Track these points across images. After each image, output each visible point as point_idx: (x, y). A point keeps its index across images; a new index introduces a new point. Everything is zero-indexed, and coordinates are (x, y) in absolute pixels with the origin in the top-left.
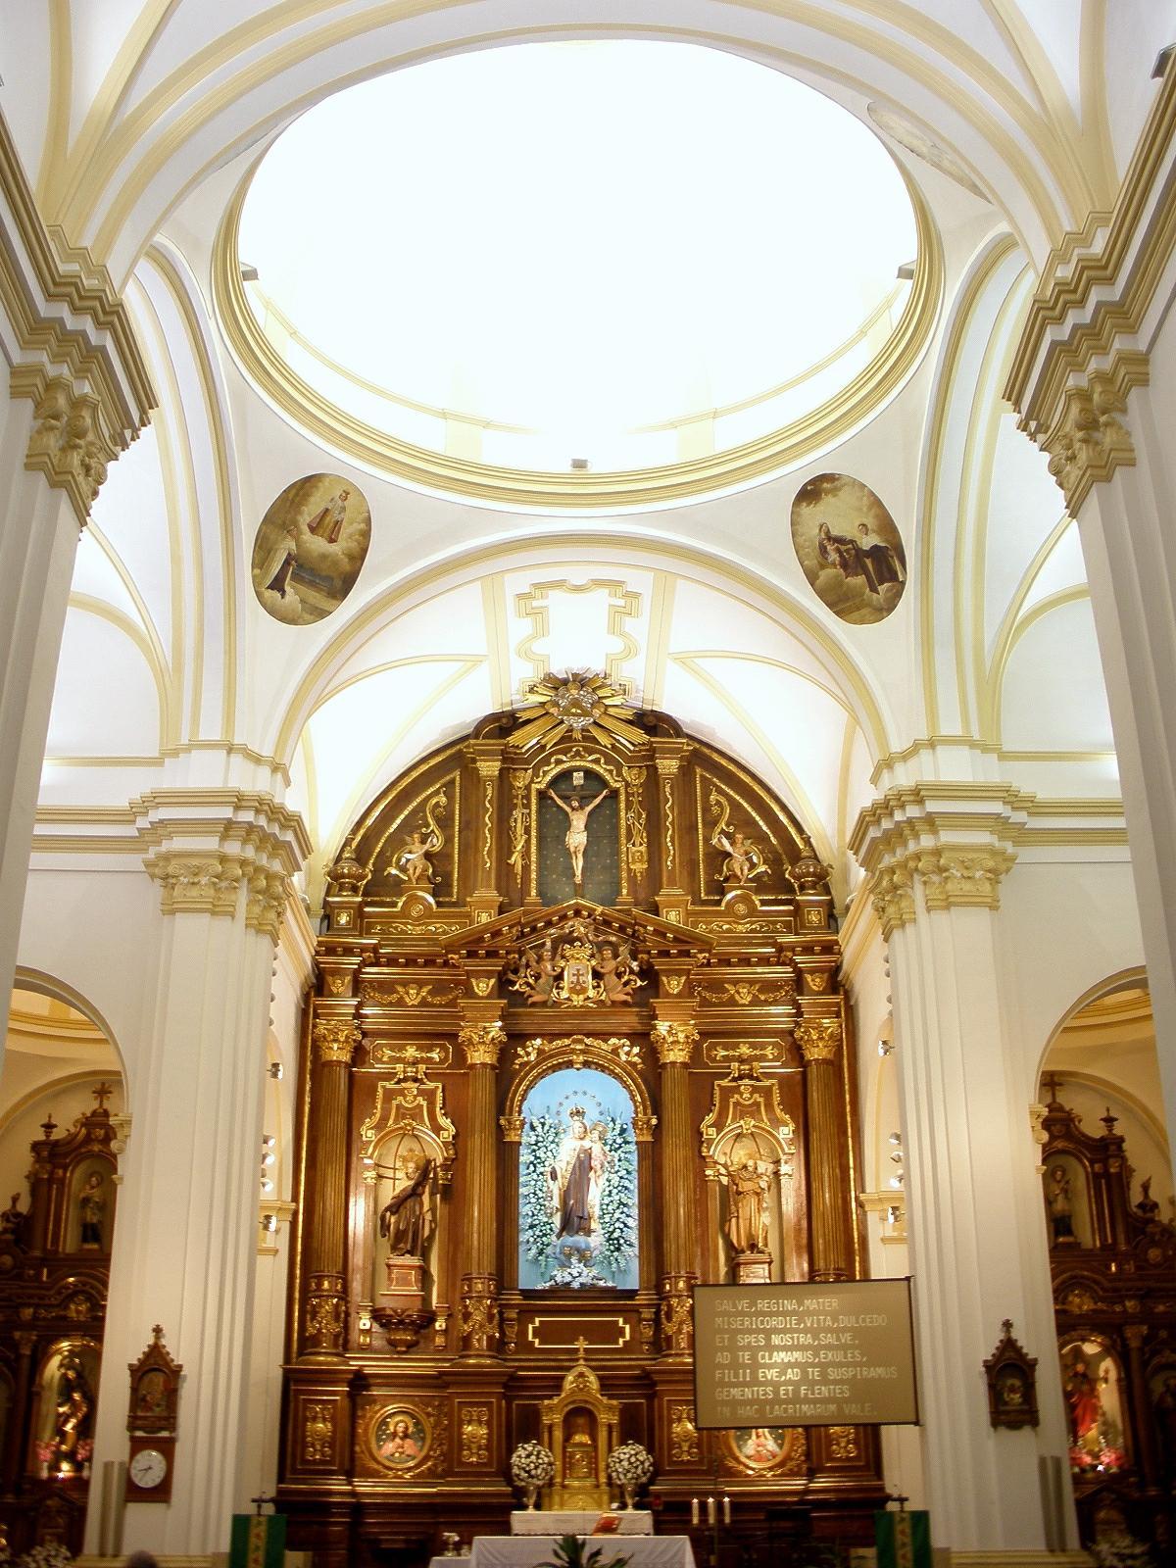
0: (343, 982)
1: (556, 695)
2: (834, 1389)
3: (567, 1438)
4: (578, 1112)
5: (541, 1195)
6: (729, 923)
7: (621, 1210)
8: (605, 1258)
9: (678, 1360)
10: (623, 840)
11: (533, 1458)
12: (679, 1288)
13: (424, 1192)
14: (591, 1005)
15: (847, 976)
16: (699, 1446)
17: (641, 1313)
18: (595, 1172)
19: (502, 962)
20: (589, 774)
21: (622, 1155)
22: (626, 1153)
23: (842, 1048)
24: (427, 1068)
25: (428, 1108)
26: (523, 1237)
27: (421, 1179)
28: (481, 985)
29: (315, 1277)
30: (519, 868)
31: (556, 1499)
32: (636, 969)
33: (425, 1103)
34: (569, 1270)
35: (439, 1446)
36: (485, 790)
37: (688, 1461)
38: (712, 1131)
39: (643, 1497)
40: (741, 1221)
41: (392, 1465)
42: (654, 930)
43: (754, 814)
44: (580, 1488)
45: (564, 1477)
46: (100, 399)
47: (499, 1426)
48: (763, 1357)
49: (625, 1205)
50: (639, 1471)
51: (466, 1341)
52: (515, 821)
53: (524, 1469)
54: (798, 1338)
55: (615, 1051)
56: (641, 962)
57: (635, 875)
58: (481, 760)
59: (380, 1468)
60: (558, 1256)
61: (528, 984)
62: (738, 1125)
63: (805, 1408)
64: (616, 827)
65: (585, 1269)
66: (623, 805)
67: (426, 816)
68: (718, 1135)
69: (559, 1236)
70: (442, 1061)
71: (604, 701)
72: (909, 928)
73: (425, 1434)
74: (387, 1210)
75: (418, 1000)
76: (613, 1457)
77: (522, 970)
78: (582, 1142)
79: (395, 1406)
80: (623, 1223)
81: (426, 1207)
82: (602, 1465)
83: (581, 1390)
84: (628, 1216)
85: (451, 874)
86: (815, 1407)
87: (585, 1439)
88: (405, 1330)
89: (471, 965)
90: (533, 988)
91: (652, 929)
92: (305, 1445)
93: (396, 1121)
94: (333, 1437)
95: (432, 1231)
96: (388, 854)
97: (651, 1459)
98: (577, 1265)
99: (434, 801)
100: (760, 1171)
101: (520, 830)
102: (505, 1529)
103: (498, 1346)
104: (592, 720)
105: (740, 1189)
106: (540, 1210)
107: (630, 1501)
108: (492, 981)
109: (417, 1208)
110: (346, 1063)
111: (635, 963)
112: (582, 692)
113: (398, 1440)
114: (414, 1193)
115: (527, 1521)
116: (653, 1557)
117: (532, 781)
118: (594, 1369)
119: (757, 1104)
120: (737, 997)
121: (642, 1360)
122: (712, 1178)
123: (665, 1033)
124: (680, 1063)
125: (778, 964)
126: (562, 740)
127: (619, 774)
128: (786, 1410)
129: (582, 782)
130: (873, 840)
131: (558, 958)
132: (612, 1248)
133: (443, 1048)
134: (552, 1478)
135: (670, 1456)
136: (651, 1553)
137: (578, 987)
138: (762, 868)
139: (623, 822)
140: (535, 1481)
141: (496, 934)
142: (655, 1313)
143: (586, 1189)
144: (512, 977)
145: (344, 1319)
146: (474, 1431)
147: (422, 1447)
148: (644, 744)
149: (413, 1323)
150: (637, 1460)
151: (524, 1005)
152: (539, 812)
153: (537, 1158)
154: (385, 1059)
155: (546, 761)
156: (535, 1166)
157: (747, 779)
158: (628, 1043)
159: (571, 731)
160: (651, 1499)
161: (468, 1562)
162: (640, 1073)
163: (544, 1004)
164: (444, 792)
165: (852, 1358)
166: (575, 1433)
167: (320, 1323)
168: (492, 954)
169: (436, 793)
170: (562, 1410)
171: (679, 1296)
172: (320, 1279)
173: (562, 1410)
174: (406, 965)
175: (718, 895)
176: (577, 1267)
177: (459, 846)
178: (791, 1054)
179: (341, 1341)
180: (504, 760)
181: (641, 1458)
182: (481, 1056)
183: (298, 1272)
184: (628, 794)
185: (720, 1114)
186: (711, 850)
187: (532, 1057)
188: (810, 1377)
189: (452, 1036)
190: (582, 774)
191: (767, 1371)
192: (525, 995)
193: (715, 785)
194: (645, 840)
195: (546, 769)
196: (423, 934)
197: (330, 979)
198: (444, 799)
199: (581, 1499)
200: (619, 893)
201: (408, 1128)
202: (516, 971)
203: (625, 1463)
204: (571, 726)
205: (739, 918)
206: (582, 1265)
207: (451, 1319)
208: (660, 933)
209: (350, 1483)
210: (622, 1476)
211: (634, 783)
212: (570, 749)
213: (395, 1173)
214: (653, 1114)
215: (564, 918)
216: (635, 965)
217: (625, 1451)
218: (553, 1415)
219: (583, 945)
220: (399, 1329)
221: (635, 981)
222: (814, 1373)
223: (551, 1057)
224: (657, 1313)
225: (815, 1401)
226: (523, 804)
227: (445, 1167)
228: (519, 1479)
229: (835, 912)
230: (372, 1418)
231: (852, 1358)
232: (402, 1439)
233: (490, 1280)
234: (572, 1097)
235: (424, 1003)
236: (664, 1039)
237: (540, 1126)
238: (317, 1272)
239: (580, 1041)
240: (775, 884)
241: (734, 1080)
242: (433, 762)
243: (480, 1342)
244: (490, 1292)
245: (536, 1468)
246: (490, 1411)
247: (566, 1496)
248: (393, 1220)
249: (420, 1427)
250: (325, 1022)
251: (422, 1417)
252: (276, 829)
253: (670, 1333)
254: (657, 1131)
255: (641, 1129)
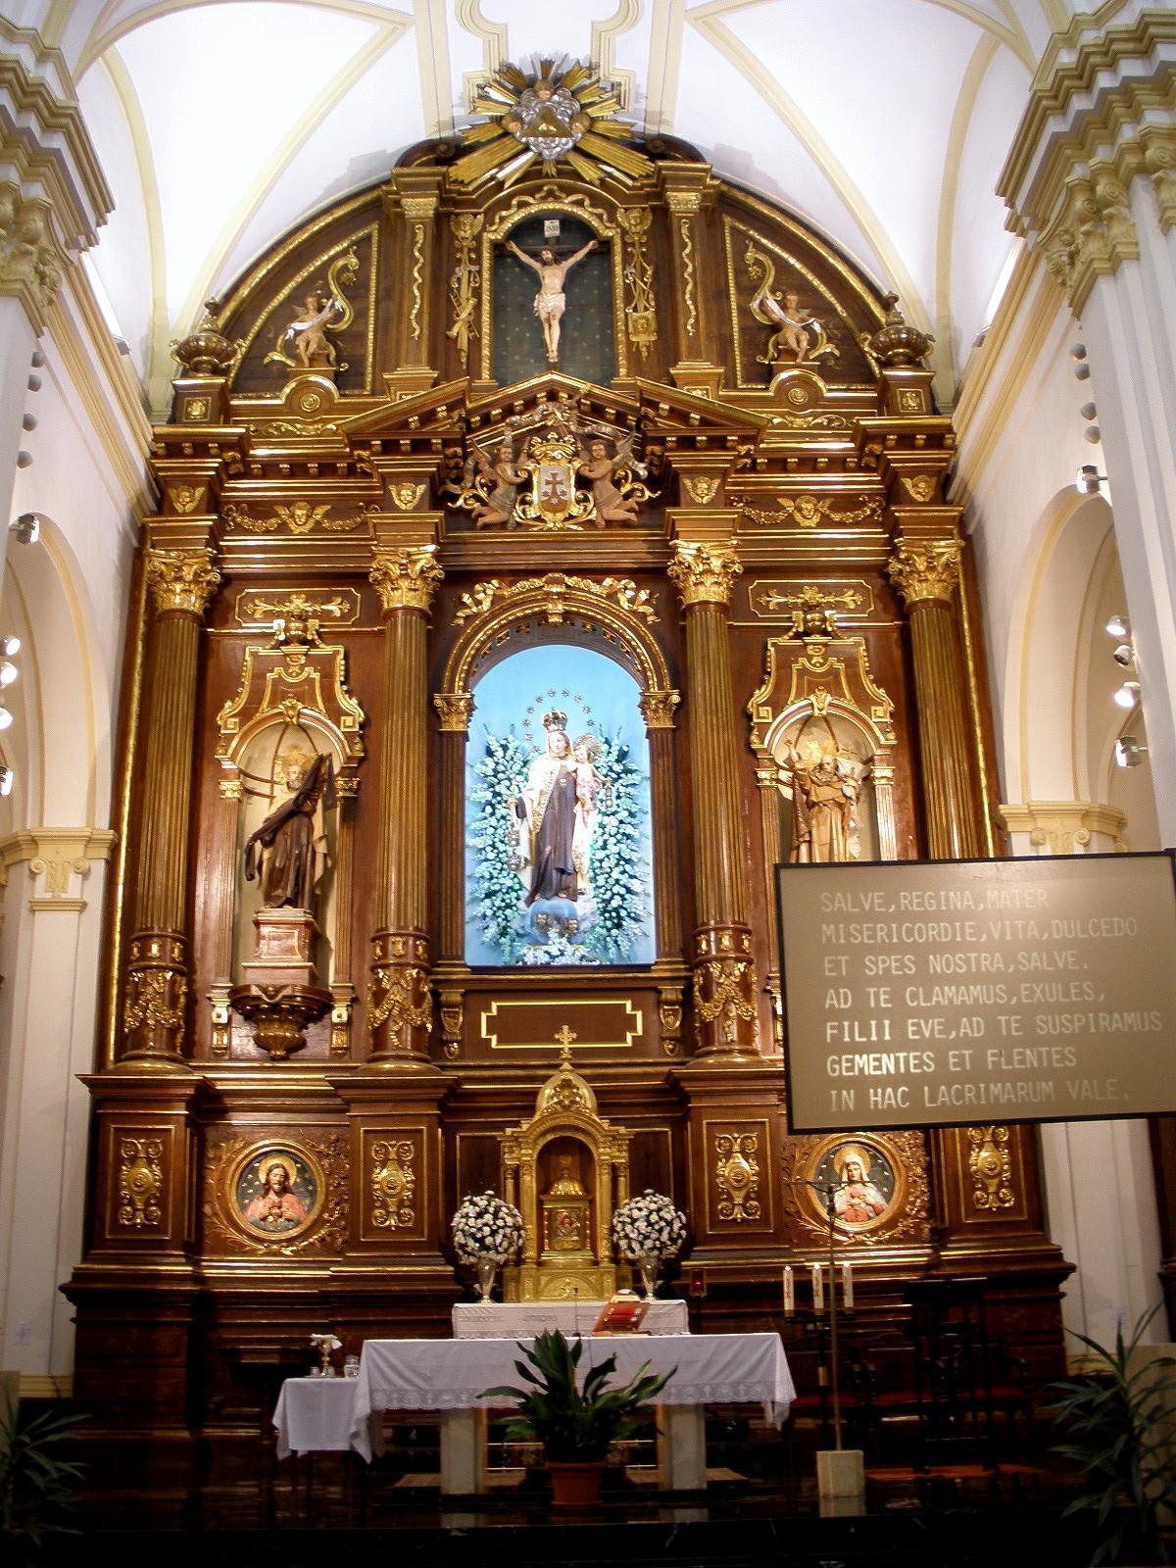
0: (192, 496)
1: (519, 104)
2: (1049, 1054)
3: (545, 1187)
4: (556, 717)
5: (502, 847)
6: (781, 415)
7: (622, 869)
8: (598, 940)
9: (724, 1059)
10: (619, 303)
11: (488, 1218)
12: (722, 947)
13: (314, 811)
14: (575, 527)
15: (965, 486)
16: (761, 1196)
17: (660, 992)
18: (583, 806)
19: (436, 459)
20: (571, 224)
21: (622, 789)
22: (627, 786)
23: (959, 593)
24: (321, 626)
25: (321, 682)
26: (471, 911)
27: (309, 786)
28: (403, 492)
29: (138, 939)
30: (463, 343)
31: (528, 1284)
32: (643, 473)
33: (316, 676)
34: (545, 948)
35: (337, 1204)
36: (414, 234)
37: (743, 1219)
38: (766, 711)
39: (670, 1280)
40: (816, 847)
41: (262, 1234)
42: (671, 408)
43: (810, 277)
44: (565, 1267)
45: (541, 1249)
46: (50, 201)
47: (432, 1168)
48: (914, 996)
49: (628, 861)
50: (665, 1236)
51: (379, 1035)
52: (459, 280)
53: (473, 1236)
54: (978, 960)
55: (612, 596)
56: (651, 464)
57: (639, 351)
58: (408, 196)
59: (245, 1239)
60: (528, 930)
61: (477, 498)
62: (806, 702)
63: (995, 1089)
64: (609, 291)
65: (568, 946)
66: (618, 259)
67: (327, 284)
68: (774, 718)
69: (530, 901)
70: (344, 617)
71: (589, 111)
72: (1130, 271)
73: (315, 1186)
74: (256, 837)
75: (310, 525)
76: (620, 1215)
77: (468, 477)
78: (563, 762)
79: (267, 1142)
80: (625, 886)
81: (318, 831)
82: (603, 1229)
83: (566, 1108)
84: (632, 877)
85: (364, 357)
86: (1014, 1087)
87: (574, 1188)
88: (281, 1022)
89: (389, 464)
90: (484, 503)
91: (667, 407)
92: (118, 1204)
93: (273, 704)
94: (164, 1190)
95: (328, 872)
96: (271, 335)
97: (684, 1218)
98: (557, 940)
99: (341, 263)
100: (842, 771)
101: (465, 292)
102: (445, 1329)
103: (431, 1045)
104: (571, 144)
105: (814, 798)
106: (502, 869)
107: (649, 1286)
108: (421, 489)
109: (304, 835)
110: (195, 615)
111: (642, 465)
112: (556, 98)
113: (272, 1196)
114: (296, 811)
115: (478, 1319)
116: (714, 1371)
117: (484, 229)
118: (588, 1079)
119: (833, 673)
120: (798, 517)
121: (663, 1061)
122: (767, 783)
123: (690, 559)
124: (716, 603)
125: (859, 469)
126: (526, 177)
127: (612, 219)
128: (960, 1094)
129: (557, 233)
130: (1056, 137)
131: (523, 458)
132: (609, 924)
133: (346, 596)
134: (520, 1251)
135: (713, 1212)
136: (709, 1364)
137: (554, 501)
138: (828, 348)
139: (619, 280)
140: (492, 1254)
141: (428, 417)
142: (683, 992)
143: (569, 831)
144: (454, 488)
145: (192, 1007)
146: (392, 1177)
147: (312, 1204)
148: (648, 176)
149: (293, 1009)
150: (661, 1218)
151: (472, 527)
152: (494, 269)
153: (496, 794)
154: (257, 616)
155: (505, 205)
156: (493, 806)
157: (800, 232)
158: (633, 585)
159: (540, 163)
160: (683, 1281)
161: (355, 1385)
162: (651, 628)
163: (503, 525)
164: (355, 253)
165: (1077, 995)
166: (558, 1180)
167: (145, 1009)
168: (421, 446)
169: (344, 253)
170: (536, 1140)
171: (722, 960)
172: (146, 940)
173: (536, 1140)
174: (292, 475)
175: (762, 382)
176: (556, 943)
177: (377, 291)
178: (881, 601)
179: (179, 1040)
180: (442, 201)
181: (668, 1217)
182: (403, 596)
183: (117, 937)
184: (625, 244)
185: (777, 687)
186: (750, 323)
187: (486, 606)
188: (1004, 1032)
189: (359, 579)
190: (557, 223)
191: (884, 1056)
192: (473, 515)
193: (752, 239)
194: (653, 304)
195: (504, 213)
196: (319, 436)
197: (173, 493)
198: (354, 260)
199: (568, 1284)
200: (616, 374)
201: (291, 713)
202: (458, 480)
203: (642, 1225)
204: (540, 154)
205: (796, 408)
206: (564, 940)
207: (356, 1007)
208: (679, 414)
209: (196, 1264)
210: (635, 1245)
211: (633, 229)
212: (539, 188)
213: (272, 788)
214: (673, 687)
215: (531, 404)
216: (642, 469)
217: (640, 1205)
218: (521, 1154)
219: (561, 438)
220: (272, 1021)
221: (642, 491)
222: (1008, 1023)
223: (515, 605)
224: (688, 992)
225: (1014, 1076)
226: (470, 259)
227: (348, 772)
228: (465, 1252)
229: (938, 405)
230: (230, 1161)
231: (1077, 995)
232: (277, 1193)
233: (417, 938)
234: (546, 698)
235: (318, 528)
236: (689, 567)
237: (500, 750)
238: (142, 930)
239: (560, 582)
240: (850, 368)
241: (798, 636)
242: (339, 213)
243: (399, 1037)
244: (417, 957)
245: (493, 1233)
246: (418, 1145)
247: (544, 1280)
248: (266, 855)
249: (307, 1176)
250: (163, 552)
251: (312, 1161)
252: (32, 123)
253: (710, 1019)
254: (681, 713)
255: (656, 711)
